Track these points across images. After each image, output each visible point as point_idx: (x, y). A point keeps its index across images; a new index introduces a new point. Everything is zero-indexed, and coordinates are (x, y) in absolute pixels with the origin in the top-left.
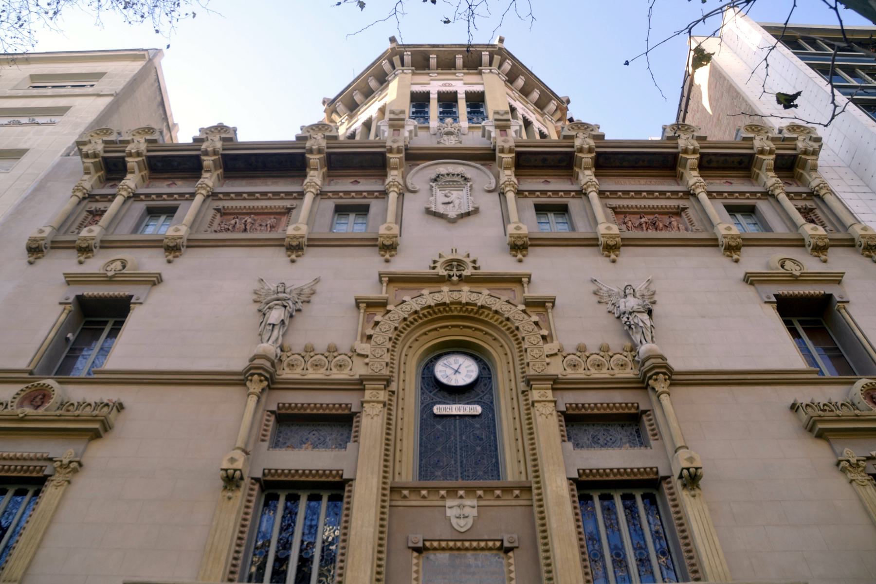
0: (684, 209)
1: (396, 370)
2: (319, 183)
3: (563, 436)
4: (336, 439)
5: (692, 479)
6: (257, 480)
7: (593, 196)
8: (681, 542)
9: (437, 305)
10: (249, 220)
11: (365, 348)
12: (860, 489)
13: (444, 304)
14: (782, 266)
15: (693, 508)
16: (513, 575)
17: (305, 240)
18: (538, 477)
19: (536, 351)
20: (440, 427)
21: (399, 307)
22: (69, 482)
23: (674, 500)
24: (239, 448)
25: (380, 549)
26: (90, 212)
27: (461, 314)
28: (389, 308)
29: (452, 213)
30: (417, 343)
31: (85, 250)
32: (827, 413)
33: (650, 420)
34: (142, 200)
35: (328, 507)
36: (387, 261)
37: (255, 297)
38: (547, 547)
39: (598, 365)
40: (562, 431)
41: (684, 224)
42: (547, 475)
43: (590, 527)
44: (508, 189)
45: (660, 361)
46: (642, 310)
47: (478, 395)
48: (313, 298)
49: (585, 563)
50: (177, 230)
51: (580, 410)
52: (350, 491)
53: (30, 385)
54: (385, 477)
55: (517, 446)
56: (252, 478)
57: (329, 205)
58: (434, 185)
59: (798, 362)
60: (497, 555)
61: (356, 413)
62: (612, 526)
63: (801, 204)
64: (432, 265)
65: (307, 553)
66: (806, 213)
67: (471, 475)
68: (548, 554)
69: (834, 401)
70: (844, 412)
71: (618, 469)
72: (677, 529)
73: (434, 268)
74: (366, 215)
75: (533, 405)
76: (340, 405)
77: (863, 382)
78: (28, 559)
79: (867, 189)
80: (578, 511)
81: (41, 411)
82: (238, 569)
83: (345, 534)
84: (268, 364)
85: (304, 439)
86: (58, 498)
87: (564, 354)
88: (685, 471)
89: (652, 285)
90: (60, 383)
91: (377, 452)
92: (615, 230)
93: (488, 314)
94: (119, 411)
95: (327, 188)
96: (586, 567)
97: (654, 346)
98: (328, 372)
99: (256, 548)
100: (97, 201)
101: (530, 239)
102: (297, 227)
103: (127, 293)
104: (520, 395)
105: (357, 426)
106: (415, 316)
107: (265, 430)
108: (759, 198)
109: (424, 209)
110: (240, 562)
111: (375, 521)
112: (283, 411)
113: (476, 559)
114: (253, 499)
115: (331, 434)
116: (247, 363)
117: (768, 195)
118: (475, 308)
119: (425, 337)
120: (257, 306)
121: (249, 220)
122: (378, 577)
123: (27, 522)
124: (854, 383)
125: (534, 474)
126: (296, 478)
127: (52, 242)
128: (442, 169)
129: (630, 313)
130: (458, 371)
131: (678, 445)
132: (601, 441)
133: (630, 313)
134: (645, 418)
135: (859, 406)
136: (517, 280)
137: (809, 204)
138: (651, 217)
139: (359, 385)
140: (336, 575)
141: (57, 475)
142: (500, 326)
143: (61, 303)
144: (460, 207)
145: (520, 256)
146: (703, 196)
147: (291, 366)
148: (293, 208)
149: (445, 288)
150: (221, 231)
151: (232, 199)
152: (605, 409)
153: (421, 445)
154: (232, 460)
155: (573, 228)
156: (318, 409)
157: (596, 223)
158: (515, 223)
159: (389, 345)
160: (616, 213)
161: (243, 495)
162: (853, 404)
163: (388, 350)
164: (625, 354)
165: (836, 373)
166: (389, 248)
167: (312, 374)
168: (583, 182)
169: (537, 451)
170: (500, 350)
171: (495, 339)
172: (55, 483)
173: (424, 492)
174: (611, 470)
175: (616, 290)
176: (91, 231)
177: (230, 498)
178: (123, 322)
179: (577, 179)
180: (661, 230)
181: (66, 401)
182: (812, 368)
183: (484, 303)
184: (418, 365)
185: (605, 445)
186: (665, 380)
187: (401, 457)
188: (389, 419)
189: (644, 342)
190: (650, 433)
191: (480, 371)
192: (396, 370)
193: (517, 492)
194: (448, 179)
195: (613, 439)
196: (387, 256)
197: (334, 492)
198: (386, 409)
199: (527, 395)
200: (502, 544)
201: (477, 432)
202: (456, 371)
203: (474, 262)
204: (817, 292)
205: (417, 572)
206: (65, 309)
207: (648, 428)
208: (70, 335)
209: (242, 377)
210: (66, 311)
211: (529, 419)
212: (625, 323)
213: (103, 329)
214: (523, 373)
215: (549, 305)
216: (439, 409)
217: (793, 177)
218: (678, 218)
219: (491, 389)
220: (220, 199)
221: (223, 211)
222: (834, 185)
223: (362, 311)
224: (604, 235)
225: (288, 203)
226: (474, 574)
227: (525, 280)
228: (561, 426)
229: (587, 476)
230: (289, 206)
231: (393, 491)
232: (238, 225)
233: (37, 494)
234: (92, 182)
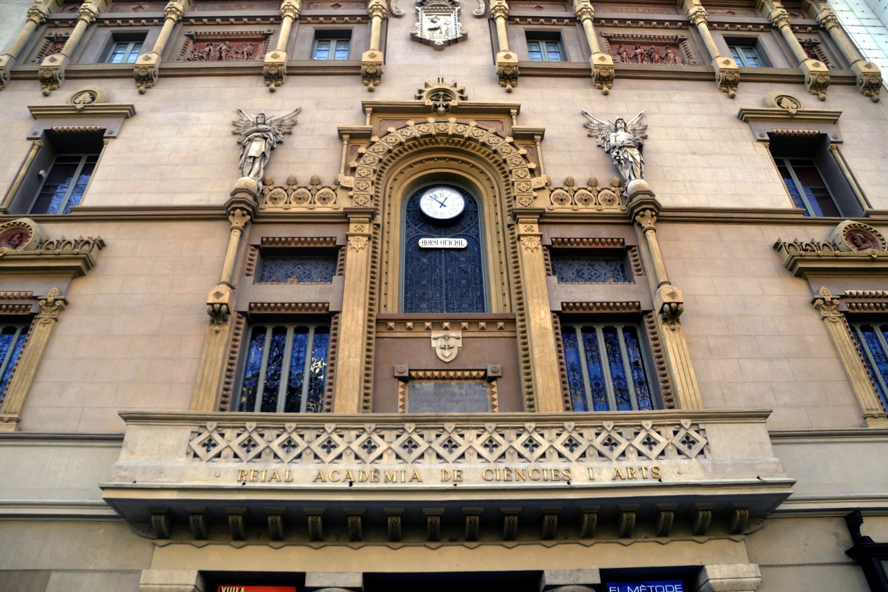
0: (682, 40)
1: (381, 203)
2: (298, 6)
3: (548, 270)
4: (321, 272)
5: (673, 314)
6: (243, 313)
7: (588, 24)
8: (659, 373)
9: (422, 136)
10: (224, 47)
11: (348, 180)
12: (831, 326)
13: (430, 135)
14: (779, 104)
15: (672, 342)
16: (495, 403)
17: (284, 68)
19: (523, 185)
21: (383, 139)
22: (56, 320)
23: (654, 333)
24: (224, 283)
25: (367, 378)
26: (50, 39)
27: (448, 146)
28: (373, 139)
29: (439, 39)
30: (402, 176)
31: (49, 81)
32: (809, 253)
33: (635, 255)
34: (107, 26)
35: (315, 341)
36: (371, 90)
37: (234, 129)
38: (529, 377)
39: (586, 200)
40: (547, 265)
41: (681, 56)
42: (531, 308)
43: (572, 358)
44: (498, 14)
45: (648, 197)
46: (632, 145)
47: (464, 228)
48: (295, 130)
49: (565, 392)
50: (148, 58)
51: (566, 244)
52: (336, 323)
53: (5, 224)
54: (370, 310)
55: (502, 279)
56: (239, 312)
57: (309, 30)
58: (420, 9)
59: (785, 202)
60: (481, 384)
61: (340, 247)
62: (593, 357)
63: (805, 37)
64: (418, 95)
65: (296, 383)
66: (811, 49)
67: (455, 307)
68: (530, 383)
69: (816, 241)
70: (825, 252)
71: (601, 303)
72: (656, 361)
73: (420, 98)
74: (348, 41)
75: (519, 239)
76: (325, 238)
77: (848, 222)
78: (25, 393)
79: (877, 23)
80: (561, 343)
81: (20, 250)
82: (229, 399)
83: (332, 365)
84: (250, 198)
85: (289, 273)
86: (47, 336)
87: (552, 188)
88: (666, 306)
89: (644, 119)
90: (35, 221)
91: (363, 285)
92: (609, 60)
94: (100, 249)
95: (307, 12)
96: (566, 395)
97: (643, 182)
98: (312, 206)
99: (245, 379)
100: (57, 27)
101: (520, 69)
102: (276, 54)
103: (99, 127)
104: (506, 229)
105: (342, 260)
106: (400, 148)
107: (250, 265)
108: (762, 31)
109: (409, 35)
110: (230, 393)
112: (268, 245)
113: (460, 388)
114: (241, 332)
115: (316, 268)
116: (229, 197)
117: (772, 27)
118: (462, 140)
119: (410, 169)
120: (236, 139)
121: (224, 47)
122: (365, 404)
123: (19, 358)
124: (838, 224)
126: (283, 311)
127: (12, 72)
129: (620, 148)
130: (444, 204)
131: (662, 280)
132: (585, 276)
133: (620, 148)
134: (630, 254)
135: (840, 246)
136: (505, 111)
137: (813, 38)
138: (647, 48)
139: (344, 218)
140: (324, 403)
141: (43, 313)
142: (487, 159)
143: (29, 139)
144: (447, 34)
145: (509, 86)
146: (703, 27)
147: (274, 199)
148: (270, 34)
149: (431, 120)
150: (194, 59)
151: (205, 24)
152: (590, 244)
153: (406, 277)
154: (218, 295)
155: (565, 58)
156: (303, 243)
157: (589, 53)
158: (504, 51)
159: (374, 178)
160: (611, 43)
161: (230, 329)
162: (834, 245)
163: (373, 183)
164: (613, 189)
165: (821, 213)
166: (372, 76)
167: (296, 208)
168: (577, 9)
170: (487, 183)
171: (482, 172)
172: (42, 320)
173: (410, 324)
174: (594, 303)
175: (607, 124)
176: (53, 60)
177: (217, 332)
178: (98, 157)
179: (572, 5)
180: (657, 62)
181: (44, 239)
182: (799, 209)
184: (402, 203)
185: (589, 280)
186: (652, 216)
187: (387, 289)
188: (374, 252)
189: (633, 177)
190: (634, 268)
191: (466, 205)
192: (381, 203)
193: (501, 324)
195: (598, 274)
196: (371, 85)
197: (321, 325)
198: (371, 242)
199: (513, 229)
200: (486, 373)
201: (463, 266)
202: (442, 205)
203: (462, 92)
204: (812, 131)
205: (403, 400)
206: (34, 145)
207: (633, 264)
208: (42, 172)
209: (224, 212)
210: (35, 147)
211: (515, 252)
212: (615, 158)
213: (77, 165)
214: (509, 206)
215: (538, 137)
217: (800, 8)
218: (675, 50)
219: (477, 222)
220: (192, 25)
221: (195, 37)
222: (842, 18)
223: (345, 142)
224: (597, 66)
225: (265, 29)
226: (458, 401)
227: (514, 111)
228: (546, 260)
229: (571, 309)
230: (266, 32)
231: (378, 323)
232: (212, 53)
233: (25, 331)
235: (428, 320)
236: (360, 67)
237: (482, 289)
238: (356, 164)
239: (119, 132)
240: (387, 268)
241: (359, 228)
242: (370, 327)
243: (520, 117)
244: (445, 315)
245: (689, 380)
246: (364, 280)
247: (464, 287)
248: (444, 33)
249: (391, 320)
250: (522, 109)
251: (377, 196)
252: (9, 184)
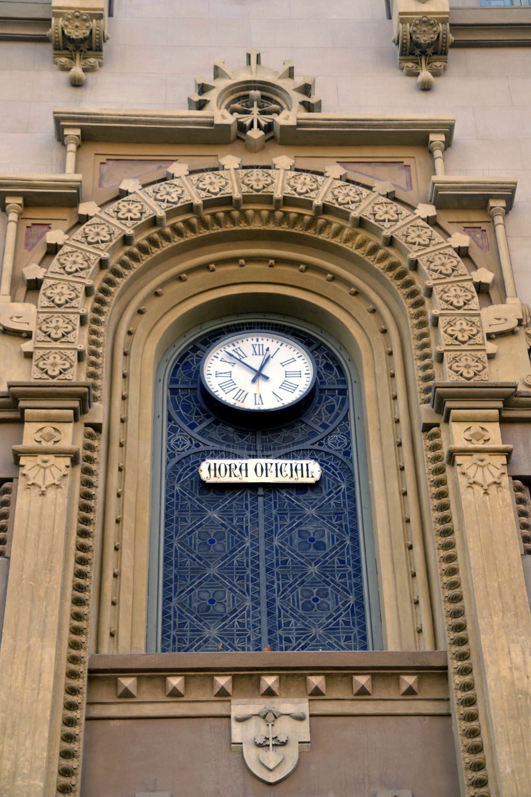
1: (103, 372)
13: (228, 201)
18: (462, 642)
19: (461, 324)
20: (215, 515)
21: (111, 209)
27: (271, 227)
28: (84, 209)
30: (157, 302)
36: (76, 84)
42: (485, 639)
47: (314, 434)
54: (74, 645)
55: (410, 562)
64: (196, 98)
67: (293, 635)
73: (201, 105)
75: (451, 460)
91: (57, 582)
93: (341, 229)
101: (455, 27)
104: (419, 436)
106: (153, 232)
111: (49, 759)
118: (308, 213)
119: (178, 286)
125: (454, 635)
130: (259, 373)
136: (416, 139)
142: (369, 259)
145: (425, 74)
149: (230, 161)
159: (86, 307)
163: (83, 320)
169: (461, 576)
170: (369, 320)
173: (175, 682)
183: (329, 198)
184: (158, 365)
187: (117, 590)
188: (87, 496)
191: (318, 375)
192: (103, 372)
193: (409, 680)
196: (77, 70)
198: (78, 470)
201: (311, 528)
203: (306, 89)
211: (442, 495)
214: (427, 379)
215: (498, 204)
216: (210, 471)
219: (346, 418)
227: (437, 138)
235: (223, 671)
236: (46, 22)
237: (359, 588)
238: (39, 273)
240: (119, 536)
241: (46, 432)
242: (72, 691)
243: (453, 152)
244: (267, 656)
246: (58, 568)
247: (313, 583)
251: (94, 353)
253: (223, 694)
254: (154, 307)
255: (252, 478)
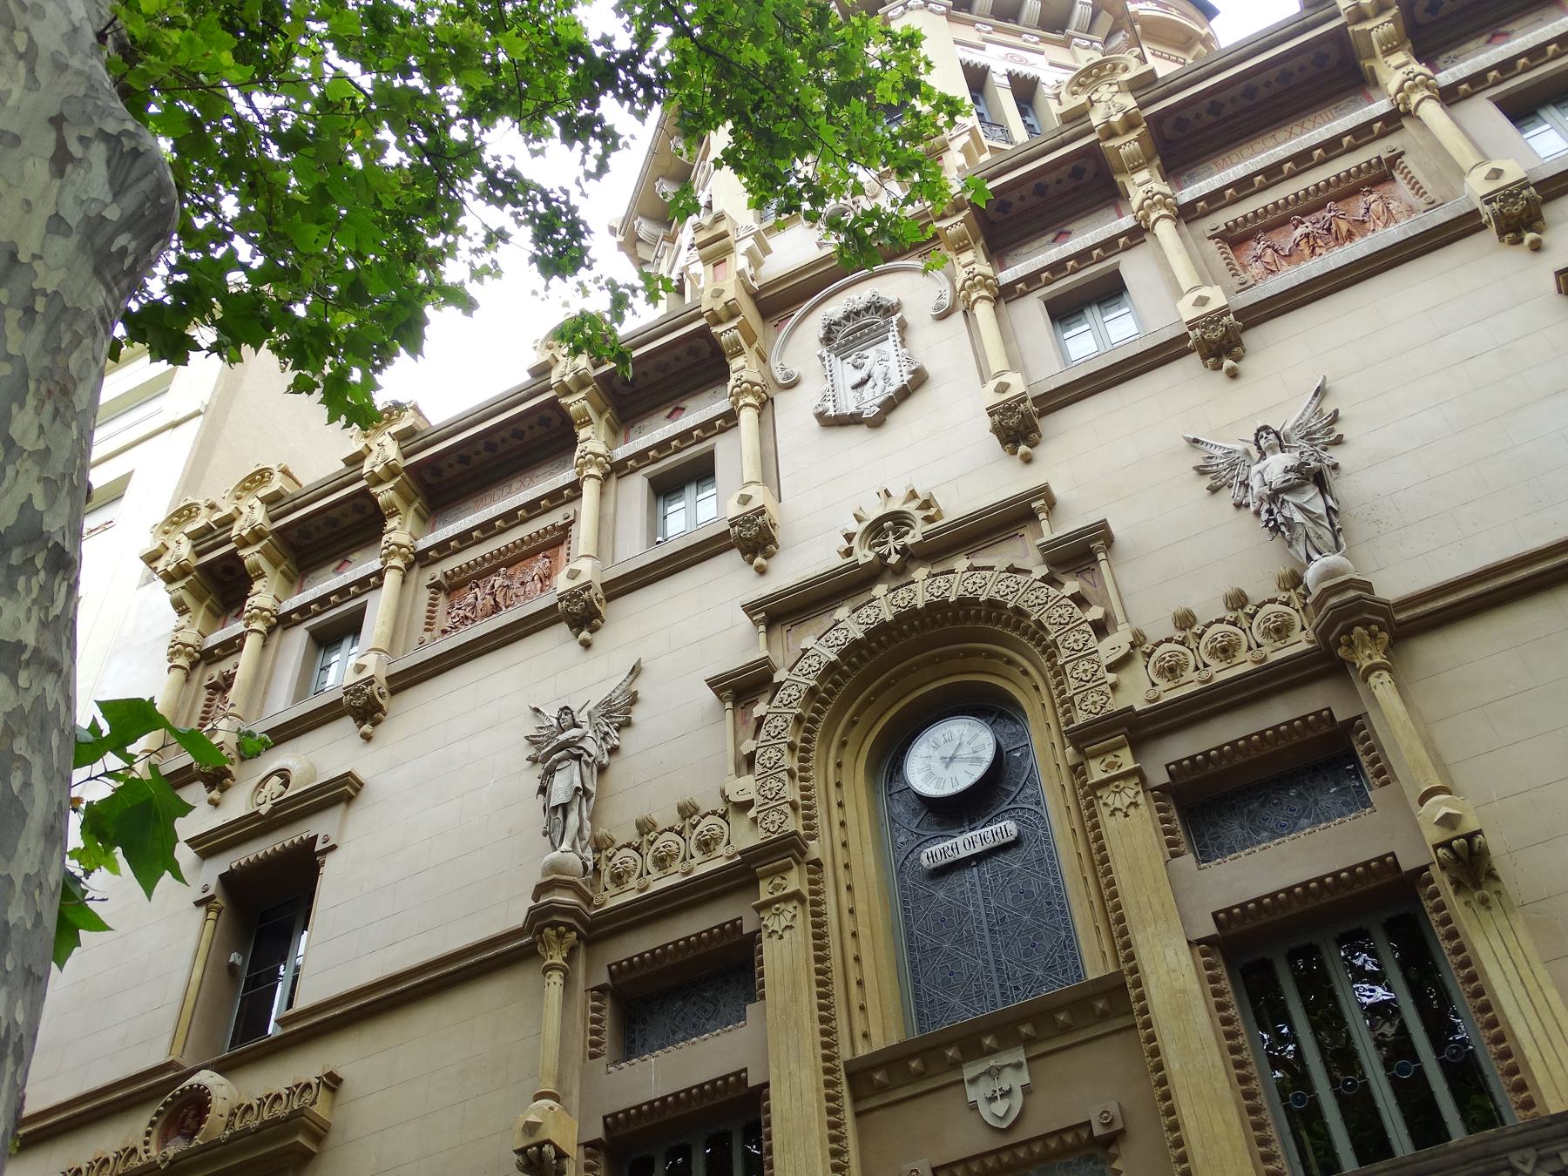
0: (1394, 160)
29: (870, 400)
37: (1207, 481)
48: (637, 714)
56: (586, 1145)
87: (1147, 647)
97: (1333, 559)
128: (835, 308)
139: (741, 877)
145: (1228, 363)
159: (791, 762)
168: (1392, 87)
180: (1350, 236)
194: (851, 326)
234: (408, 528)
239: (340, 834)
245: (1550, 1024)
248: (881, 383)
249: (1059, 1009)
250: (1056, 491)
252: (177, 1006)
253: (956, 1065)
254: (852, 737)
255: (964, 853)
